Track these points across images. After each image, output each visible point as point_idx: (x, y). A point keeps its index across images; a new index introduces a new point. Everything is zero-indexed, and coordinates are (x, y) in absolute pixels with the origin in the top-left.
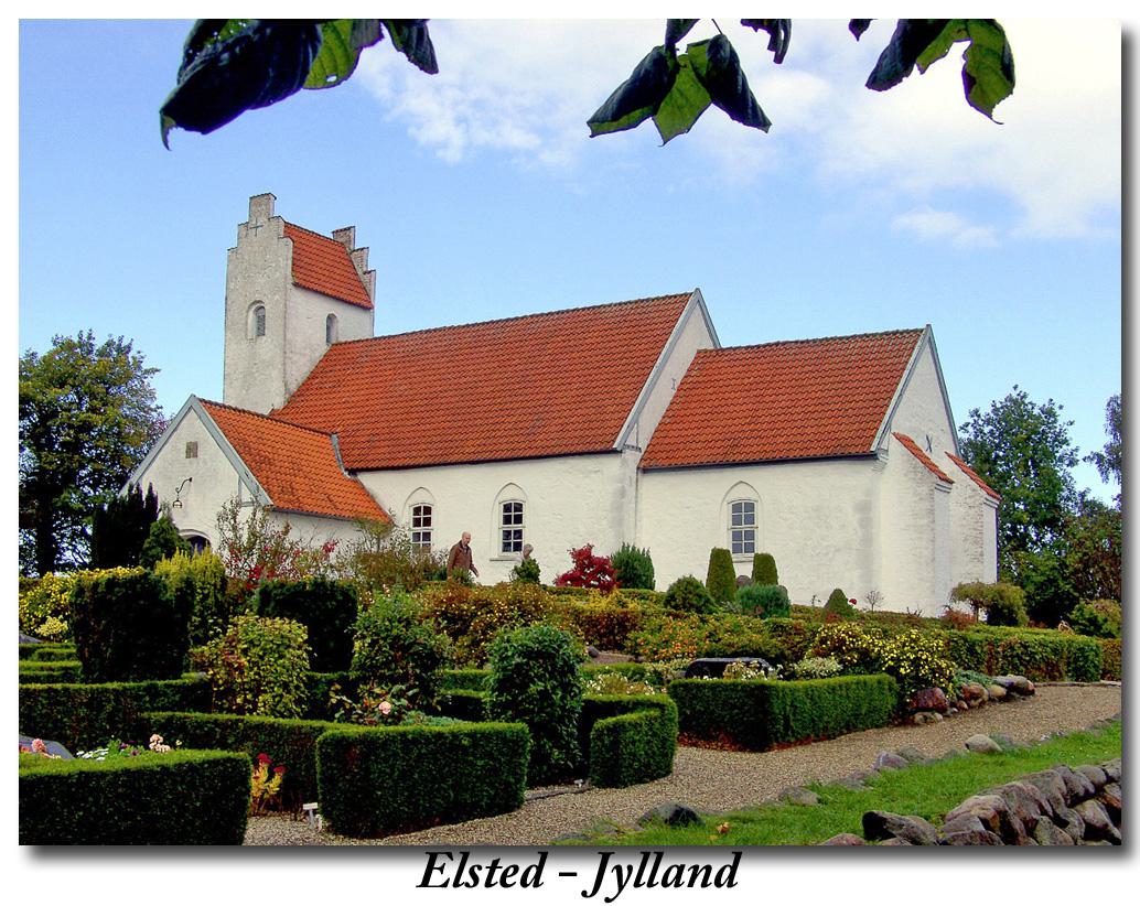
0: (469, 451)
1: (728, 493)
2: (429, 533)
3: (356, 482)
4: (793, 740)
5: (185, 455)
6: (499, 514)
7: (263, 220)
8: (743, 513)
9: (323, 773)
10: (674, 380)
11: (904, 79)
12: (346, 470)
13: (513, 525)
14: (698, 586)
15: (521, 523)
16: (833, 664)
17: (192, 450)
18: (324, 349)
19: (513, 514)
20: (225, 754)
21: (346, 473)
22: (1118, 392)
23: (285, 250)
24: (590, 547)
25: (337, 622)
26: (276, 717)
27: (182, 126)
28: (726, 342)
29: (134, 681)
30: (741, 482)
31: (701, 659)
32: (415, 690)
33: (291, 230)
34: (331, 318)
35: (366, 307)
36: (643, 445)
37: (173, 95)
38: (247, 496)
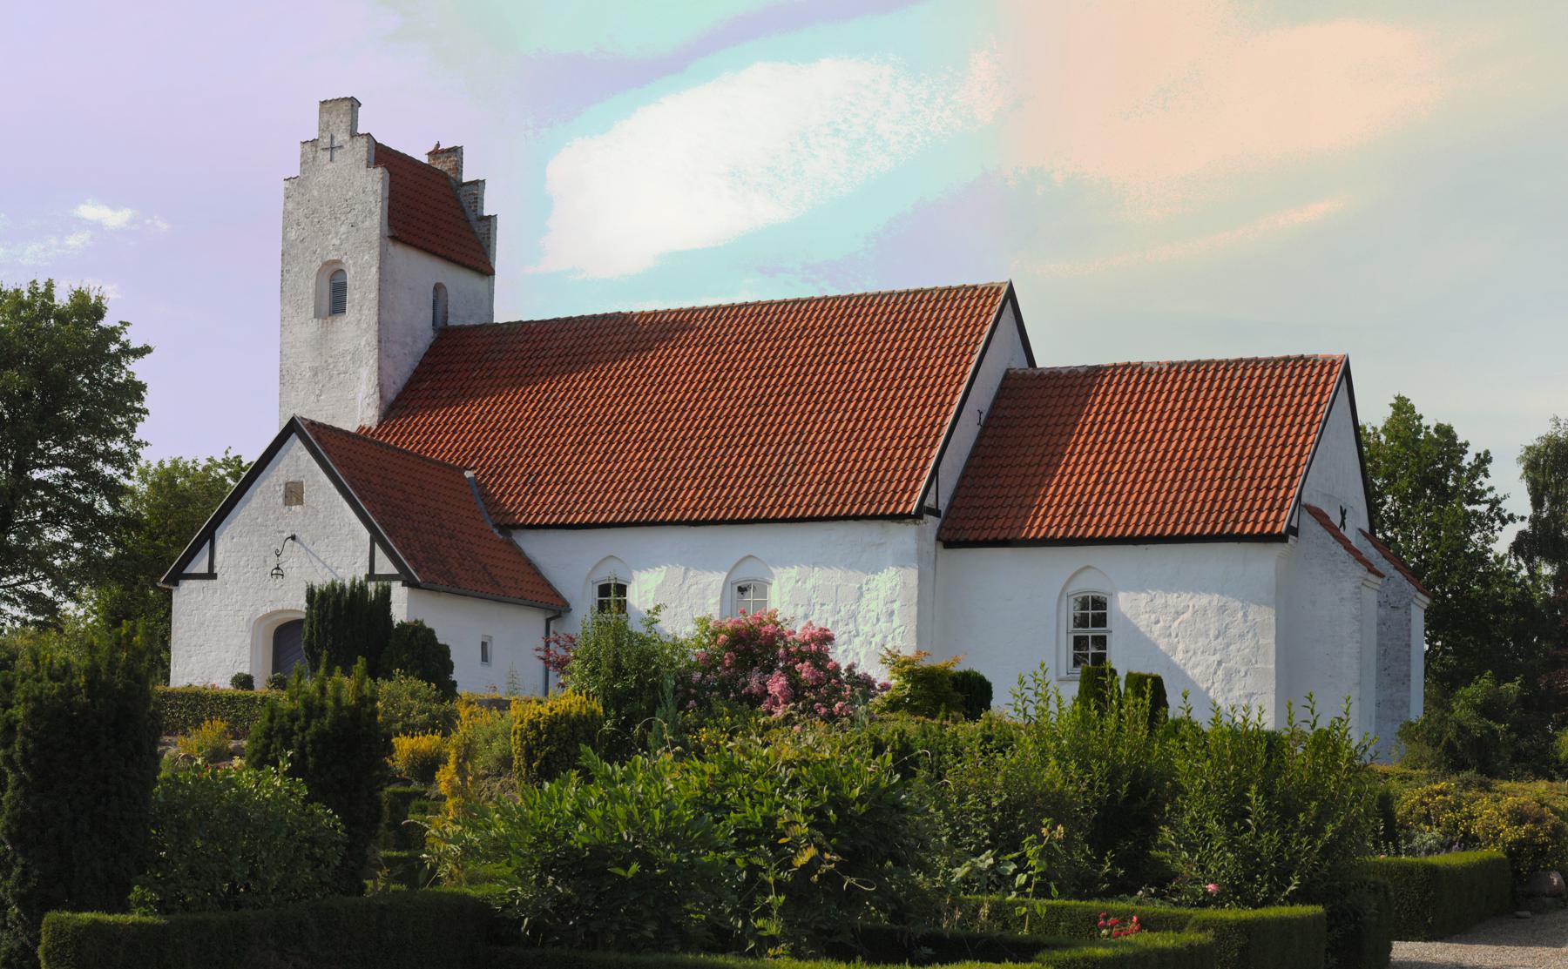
0: (686, 503)
1: (1075, 575)
2: (1104, 638)
3: (512, 544)
4: (293, 235)
5: (281, 500)
6: (1070, 611)
7: (342, 137)
8: (1093, 612)
9: (1475, 513)
10: (981, 413)
11: (441, 641)
12: (496, 526)
13: (1090, 629)
14: (1502, 859)
15: (1105, 625)
16: (990, 851)
17: (294, 494)
18: (426, 336)
19: (1090, 612)
20: (1249, 914)
21: (496, 531)
22: (251, 456)
23: (373, 183)
24: (826, 638)
25: (13, 536)
26: (675, 692)
27: (989, 703)
28: (1046, 358)
29: (1429, 657)
30: (750, 556)
31: (1286, 911)
32: (626, 838)
33: (383, 156)
34: (438, 288)
35: (484, 268)
36: (943, 506)
37: (386, 203)
38: (1237, 677)
